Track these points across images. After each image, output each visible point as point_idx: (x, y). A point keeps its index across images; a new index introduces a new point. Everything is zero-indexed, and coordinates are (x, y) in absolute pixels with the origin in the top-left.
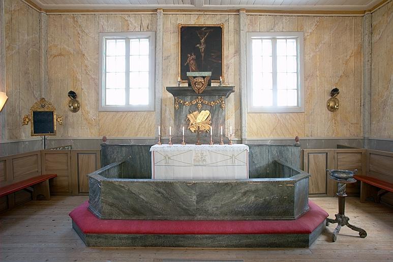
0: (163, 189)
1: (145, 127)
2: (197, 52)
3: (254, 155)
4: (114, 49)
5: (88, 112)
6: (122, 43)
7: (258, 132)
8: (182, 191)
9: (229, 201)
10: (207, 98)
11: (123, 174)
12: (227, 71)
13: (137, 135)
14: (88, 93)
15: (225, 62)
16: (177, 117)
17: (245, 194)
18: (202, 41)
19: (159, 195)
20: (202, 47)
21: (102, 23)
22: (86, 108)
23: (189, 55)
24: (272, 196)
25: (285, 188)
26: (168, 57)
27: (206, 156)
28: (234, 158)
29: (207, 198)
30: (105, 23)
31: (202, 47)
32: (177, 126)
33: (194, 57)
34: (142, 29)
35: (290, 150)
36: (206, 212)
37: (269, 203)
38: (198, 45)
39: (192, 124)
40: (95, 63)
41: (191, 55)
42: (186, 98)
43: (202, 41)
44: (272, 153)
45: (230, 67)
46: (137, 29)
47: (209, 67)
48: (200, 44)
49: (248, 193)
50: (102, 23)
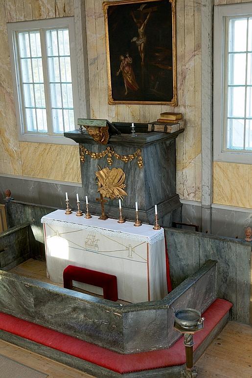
0: (7, 284)
1: (73, 168)
2: (132, 50)
3: (178, 246)
4: (29, 43)
5: (8, 141)
6: (36, 37)
7: (234, 196)
8: (22, 291)
9: (61, 312)
10: (119, 150)
11: (28, 240)
12: (181, 84)
13: (64, 178)
14: (5, 113)
15: (179, 67)
16: (84, 173)
17: (75, 309)
18: (141, 30)
19: (5, 289)
20: (140, 42)
21: (8, 7)
22: (6, 134)
23: (122, 58)
24: (101, 321)
25: (113, 316)
26: (95, 59)
27: (97, 240)
28: (130, 250)
29: (42, 304)
30: (12, 7)
31: (140, 42)
32: (85, 186)
33: (129, 60)
34: (57, 13)
35: (233, 247)
36: (43, 317)
37: (98, 326)
38: (135, 39)
39: (102, 186)
40: (8, 69)
41: (126, 57)
42: (92, 146)
43: (141, 30)
44: (205, 248)
45: (187, 77)
46: (52, 15)
47: (152, 78)
48: (138, 36)
49: (78, 310)
50: (8, 7)
